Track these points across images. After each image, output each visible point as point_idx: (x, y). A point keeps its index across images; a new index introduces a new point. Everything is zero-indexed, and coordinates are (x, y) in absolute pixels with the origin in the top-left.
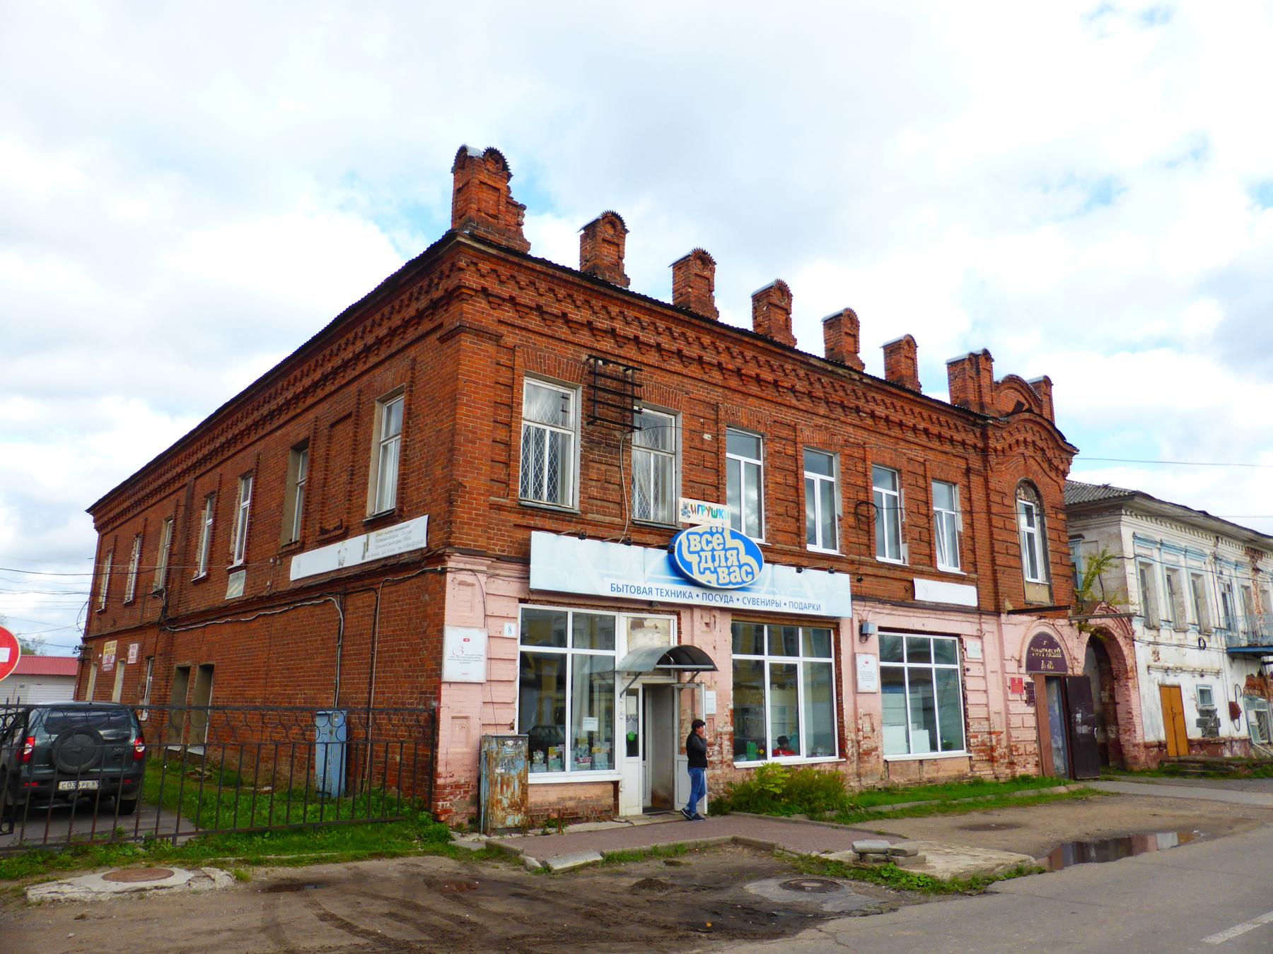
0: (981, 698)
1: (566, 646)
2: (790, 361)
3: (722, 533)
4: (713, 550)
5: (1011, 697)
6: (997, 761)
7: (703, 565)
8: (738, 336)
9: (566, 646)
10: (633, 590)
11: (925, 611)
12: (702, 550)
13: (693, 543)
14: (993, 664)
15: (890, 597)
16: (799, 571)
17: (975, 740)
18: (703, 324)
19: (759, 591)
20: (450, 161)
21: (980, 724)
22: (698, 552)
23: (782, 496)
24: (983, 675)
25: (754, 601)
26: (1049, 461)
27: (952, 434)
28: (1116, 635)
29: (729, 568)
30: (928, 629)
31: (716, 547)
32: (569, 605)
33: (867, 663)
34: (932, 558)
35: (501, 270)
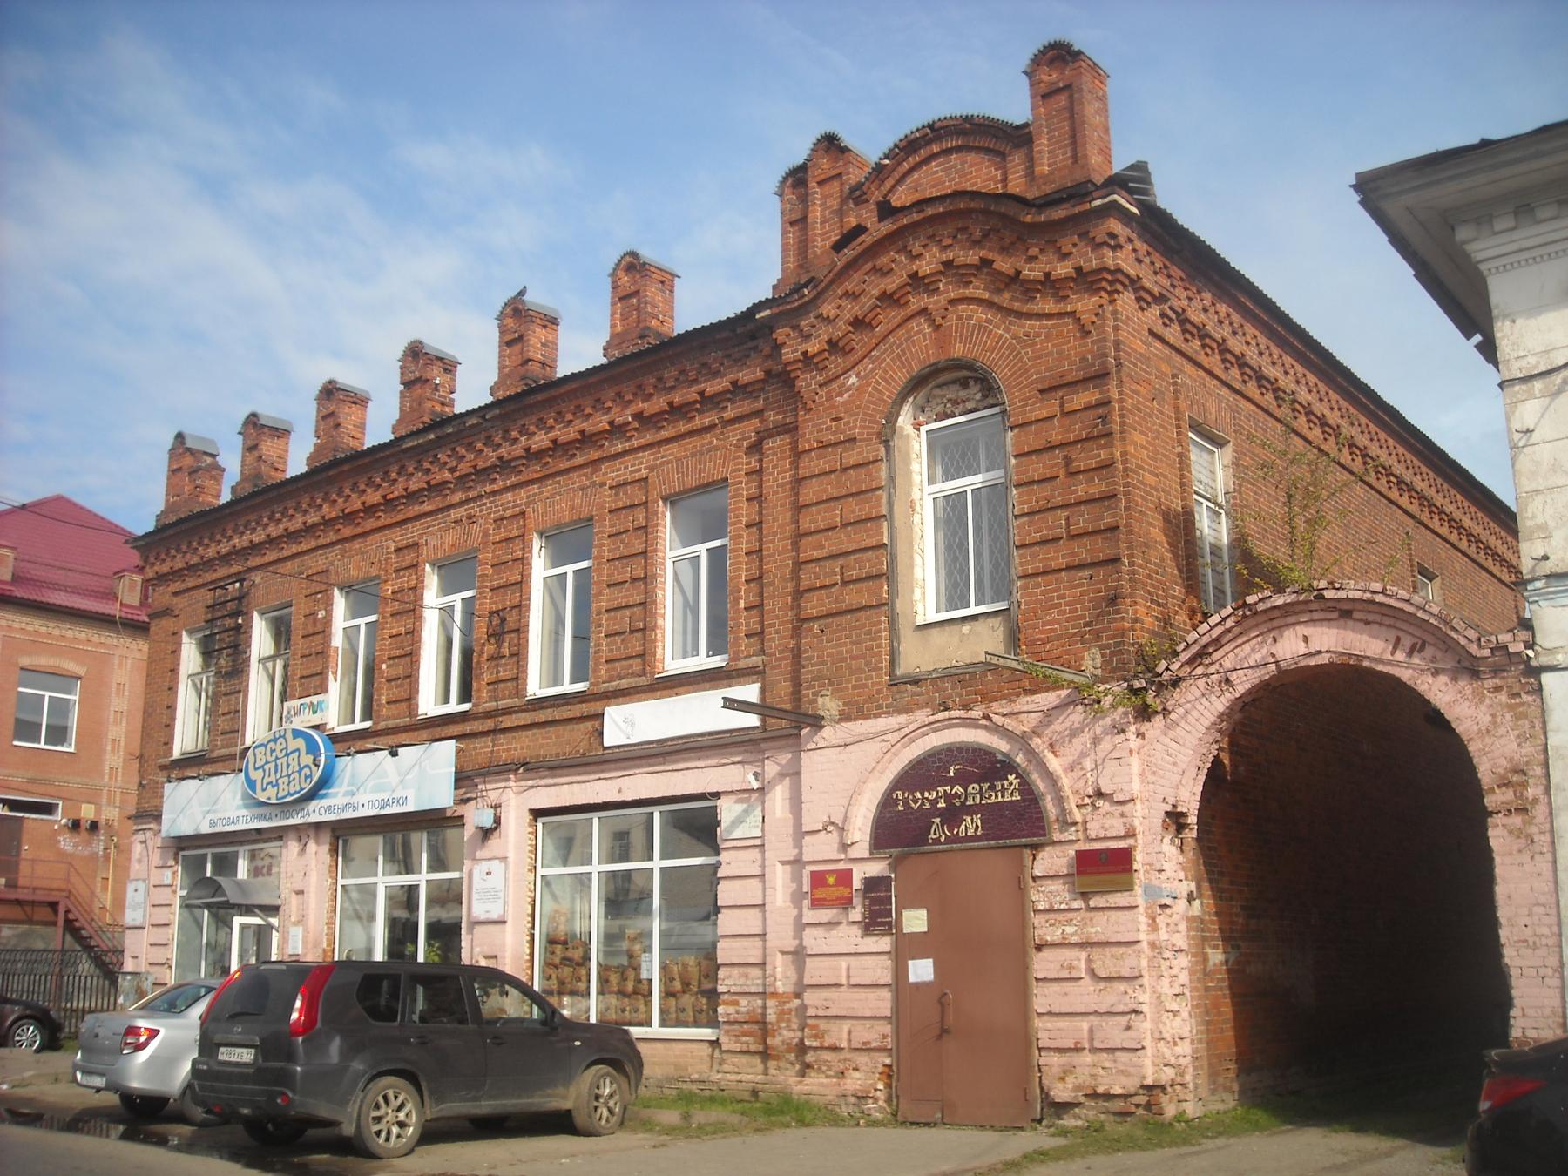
0: (749, 922)
1: (662, 858)
2: (392, 460)
3: (284, 737)
4: (277, 758)
5: (810, 916)
6: (777, 1058)
7: (267, 780)
8: (158, 537)
9: (662, 858)
10: (322, 810)
11: (588, 769)
12: (267, 762)
13: (258, 757)
14: (780, 847)
15: (557, 754)
16: (394, 754)
17: (731, 1010)
18: (266, 497)
19: (335, 795)
20: (399, 350)
21: (746, 976)
22: (262, 767)
23: (398, 652)
24: (758, 871)
25: (330, 809)
26: (1015, 279)
27: (732, 377)
28: (1405, 675)
29: (289, 776)
30: (629, 797)
31: (280, 755)
32: (209, 846)
33: (489, 873)
34: (646, 656)
35: (849, 286)
